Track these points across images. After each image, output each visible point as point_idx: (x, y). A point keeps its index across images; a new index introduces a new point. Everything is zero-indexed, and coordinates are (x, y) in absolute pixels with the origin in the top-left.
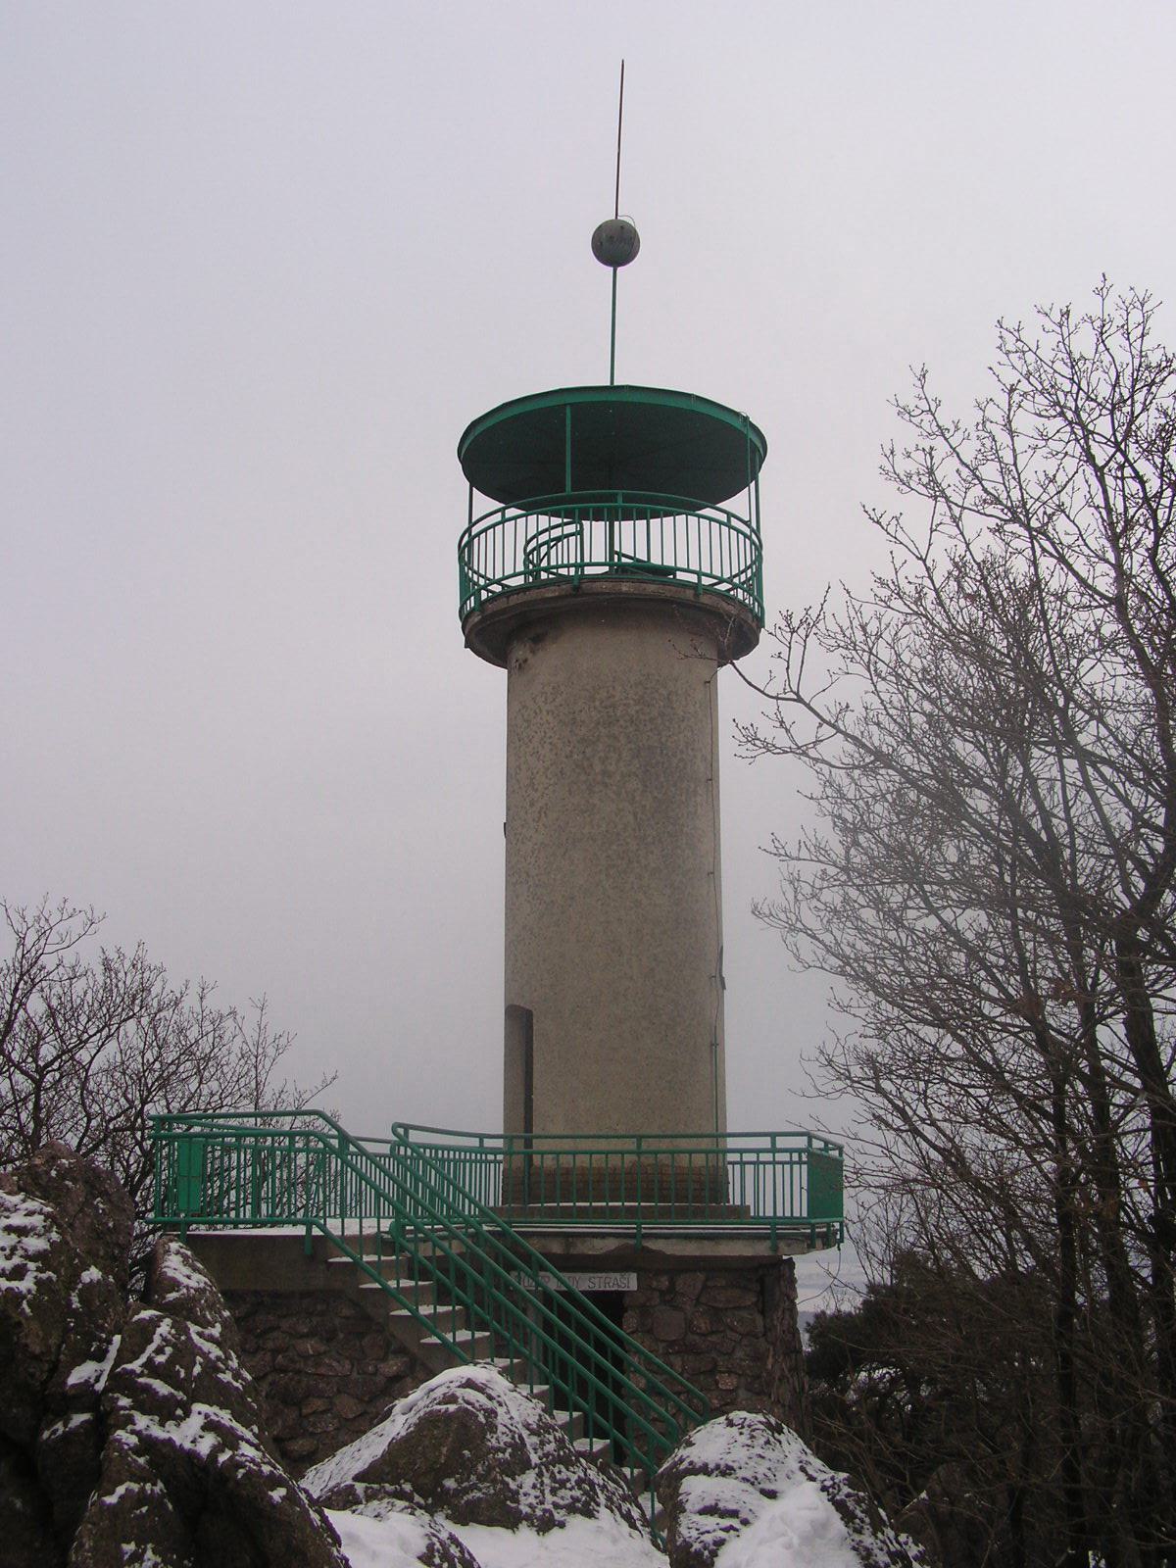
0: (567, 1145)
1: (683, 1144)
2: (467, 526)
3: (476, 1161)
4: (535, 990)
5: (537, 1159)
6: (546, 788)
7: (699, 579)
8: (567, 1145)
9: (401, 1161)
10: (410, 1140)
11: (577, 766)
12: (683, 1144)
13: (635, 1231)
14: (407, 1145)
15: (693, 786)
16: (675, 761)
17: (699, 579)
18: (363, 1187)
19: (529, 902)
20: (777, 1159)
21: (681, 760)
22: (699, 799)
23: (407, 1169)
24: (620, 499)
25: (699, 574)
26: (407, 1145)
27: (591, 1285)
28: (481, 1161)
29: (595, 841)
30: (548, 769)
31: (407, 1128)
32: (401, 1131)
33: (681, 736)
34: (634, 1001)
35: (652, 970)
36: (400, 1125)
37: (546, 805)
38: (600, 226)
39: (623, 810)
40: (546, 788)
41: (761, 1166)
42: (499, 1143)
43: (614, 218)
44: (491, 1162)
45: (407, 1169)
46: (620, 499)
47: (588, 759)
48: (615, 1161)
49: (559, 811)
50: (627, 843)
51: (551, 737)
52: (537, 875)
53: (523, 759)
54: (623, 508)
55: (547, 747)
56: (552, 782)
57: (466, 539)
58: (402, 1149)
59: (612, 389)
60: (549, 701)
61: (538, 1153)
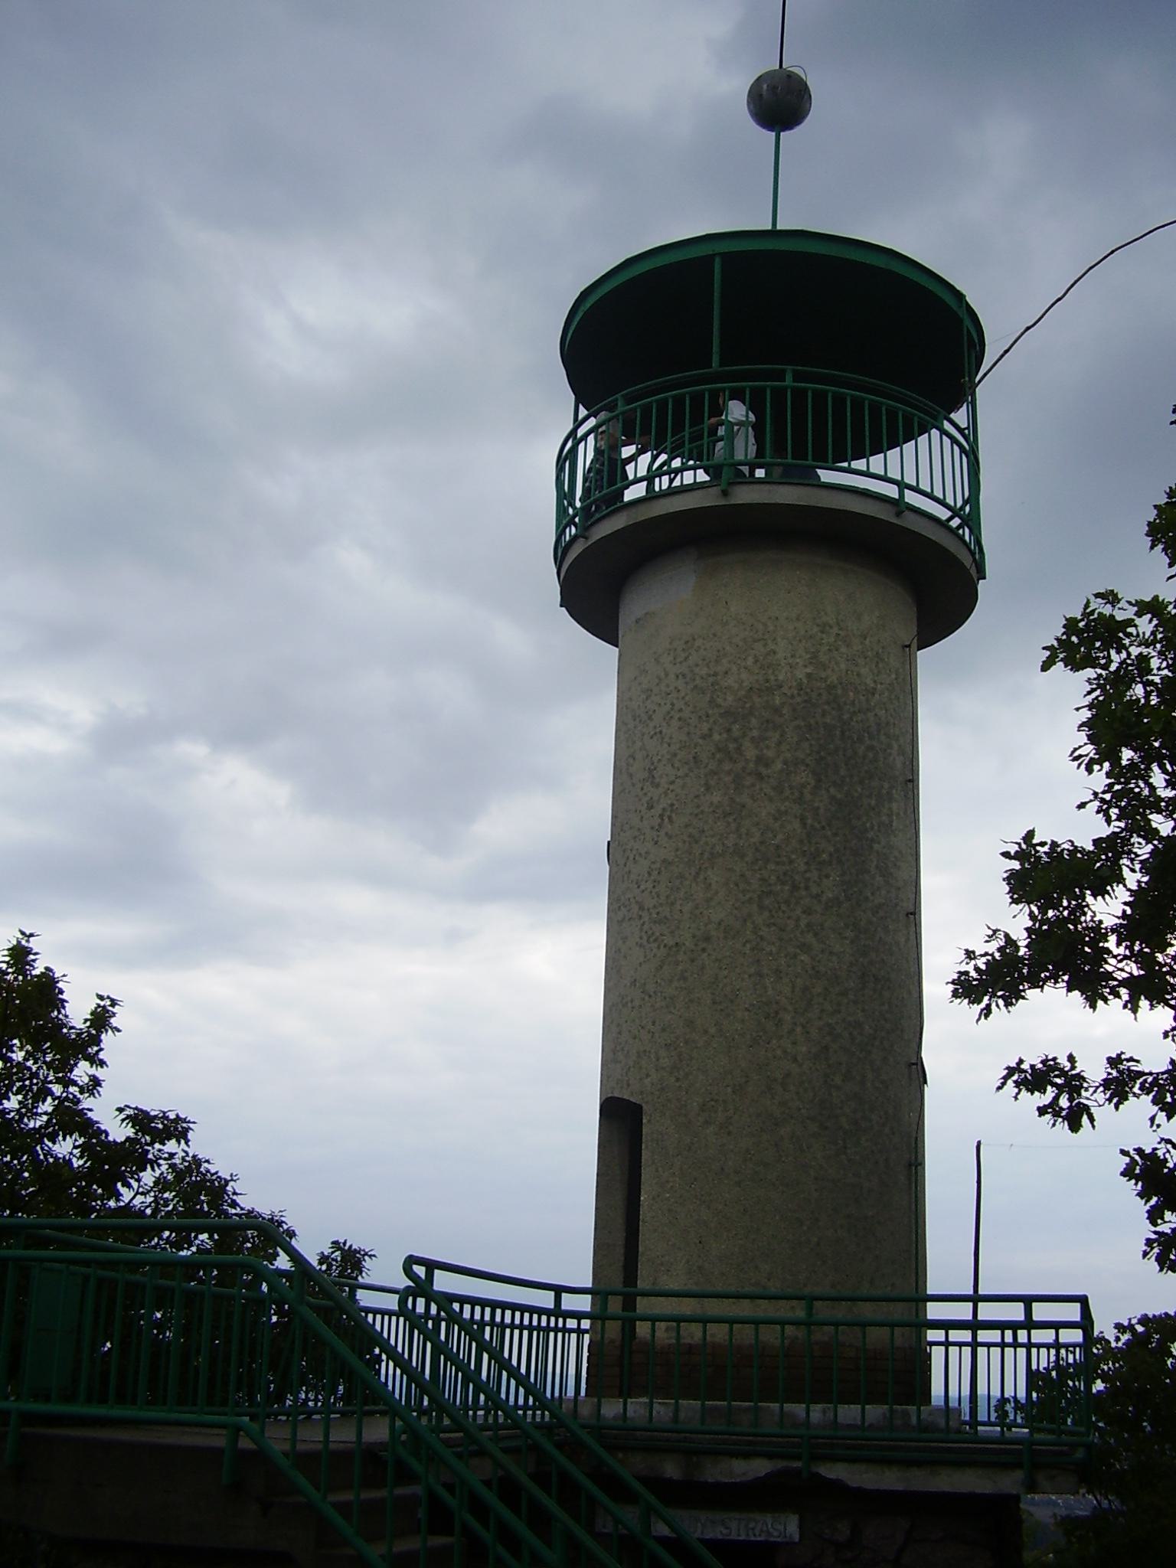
0: (687, 1307)
1: (867, 1310)
2: (571, 426)
3: (548, 1329)
4: (648, 1076)
5: (642, 1329)
6: (672, 783)
7: (901, 494)
8: (687, 1307)
9: (415, 1322)
10: (435, 1288)
11: (719, 750)
12: (867, 1310)
13: (500, 1329)
14: (431, 1296)
15: (886, 785)
16: (861, 749)
17: (901, 494)
18: (391, 1372)
19: (641, 946)
20: (951, 1339)
21: (871, 748)
22: (894, 806)
23: (483, 1347)
24: (789, 377)
25: (901, 485)
26: (431, 1296)
27: (725, 1531)
28: (556, 1330)
29: (742, 856)
30: (675, 755)
31: (431, 1266)
32: (420, 1271)
33: (870, 715)
34: (798, 1093)
35: (826, 1048)
36: (420, 1261)
37: (672, 805)
38: (761, 76)
39: (786, 812)
40: (672, 783)
41: (1034, 1351)
42: (584, 1303)
43: (778, 67)
44: (571, 1331)
45: (483, 1347)
46: (789, 377)
47: (736, 740)
48: (770, 1336)
49: (691, 814)
50: (791, 862)
51: (681, 710)
52: (655, 907)
53: (639, 744)
54: (794, 390)
55: (675, 723)
56: (680, 774)
57: (569, 444)
58: (421, 1302)
59: (774, 234)
60: (678, 660)
61: (643, 1319)
